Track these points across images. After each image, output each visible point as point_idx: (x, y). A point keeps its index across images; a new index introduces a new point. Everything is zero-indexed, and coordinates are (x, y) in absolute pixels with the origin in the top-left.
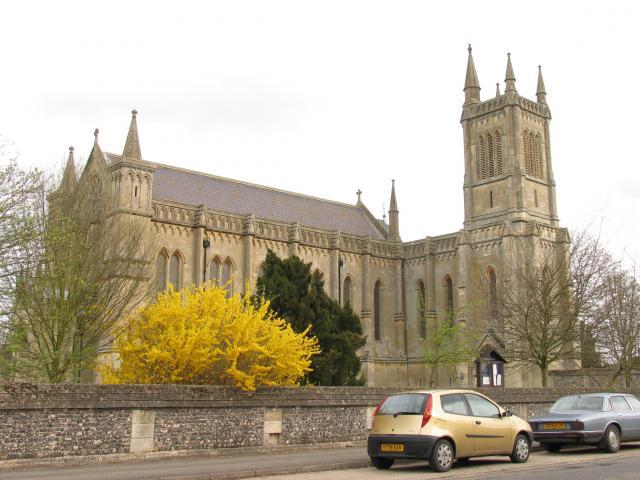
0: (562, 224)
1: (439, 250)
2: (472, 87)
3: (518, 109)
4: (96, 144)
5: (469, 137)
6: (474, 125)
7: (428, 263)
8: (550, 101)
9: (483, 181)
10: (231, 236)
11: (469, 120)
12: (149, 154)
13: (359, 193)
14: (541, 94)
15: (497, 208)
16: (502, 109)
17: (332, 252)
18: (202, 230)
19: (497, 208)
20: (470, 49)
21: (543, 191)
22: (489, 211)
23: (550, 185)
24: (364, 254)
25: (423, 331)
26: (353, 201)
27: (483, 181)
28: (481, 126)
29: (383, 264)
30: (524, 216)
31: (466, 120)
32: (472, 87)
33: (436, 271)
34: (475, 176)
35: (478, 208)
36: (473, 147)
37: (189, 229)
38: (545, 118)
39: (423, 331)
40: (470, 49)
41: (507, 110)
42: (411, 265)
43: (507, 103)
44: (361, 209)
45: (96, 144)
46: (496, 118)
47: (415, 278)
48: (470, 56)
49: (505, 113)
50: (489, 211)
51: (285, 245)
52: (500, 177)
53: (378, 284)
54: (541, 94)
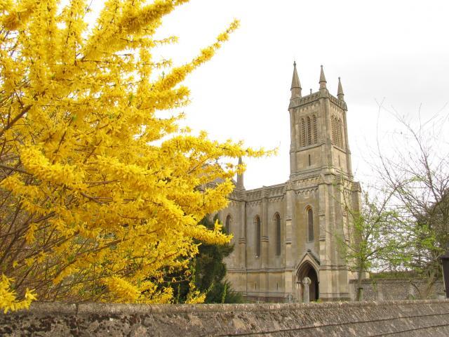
0: (355, 180)
2: (296, 87)
6: (298, 112)
8: (346, 98)
15: (314, 166)
19: (314, 166)
20: (295, 65)
21: (343, 156)
22: (308, 168)
23: (348, 153)
28: (303, 112)
31: (293, 109)
40: (295, 65)
43: (320, 97)
46: (313, 107)
54: (340, 94)
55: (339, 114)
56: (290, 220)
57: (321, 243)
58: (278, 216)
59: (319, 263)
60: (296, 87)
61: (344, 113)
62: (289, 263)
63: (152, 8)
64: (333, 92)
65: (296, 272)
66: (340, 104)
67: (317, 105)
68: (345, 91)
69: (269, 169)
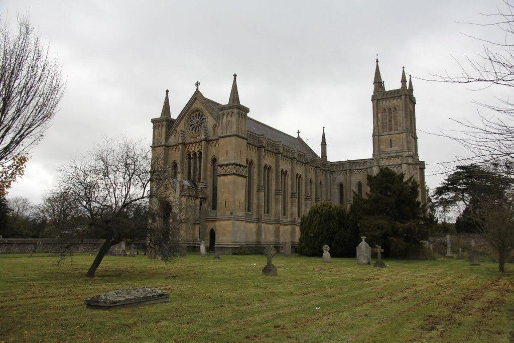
1: (354, 168)
2: (378, 82)
5: (377, 109)
6: (381, 103)
9: (386, 133)
11: (378, 100)
15: (395, 149)
16: (401, 96)
17: (306, 165)
18: (263, 149)
19: (395, 149)
20: (377, 62)
22: (389, 149)
24: (185, 145)
25: (93, 304)
27: (386, 133)
28: (384, 104)
32: (378, 82)
33: (352, 179)
34: (381, 130)
35: (382, 147)
36: (380, 115)
37: (256, 148)
39: (93, 304)
40: (377, 62)
41: (403, 97)
42: (334, 175)
46: (395, 101)
47: (337, 181)
48: (377, 66)
49: (401, 98)
50: (389, 149)
51: (274, 154)
53: (310, 181)
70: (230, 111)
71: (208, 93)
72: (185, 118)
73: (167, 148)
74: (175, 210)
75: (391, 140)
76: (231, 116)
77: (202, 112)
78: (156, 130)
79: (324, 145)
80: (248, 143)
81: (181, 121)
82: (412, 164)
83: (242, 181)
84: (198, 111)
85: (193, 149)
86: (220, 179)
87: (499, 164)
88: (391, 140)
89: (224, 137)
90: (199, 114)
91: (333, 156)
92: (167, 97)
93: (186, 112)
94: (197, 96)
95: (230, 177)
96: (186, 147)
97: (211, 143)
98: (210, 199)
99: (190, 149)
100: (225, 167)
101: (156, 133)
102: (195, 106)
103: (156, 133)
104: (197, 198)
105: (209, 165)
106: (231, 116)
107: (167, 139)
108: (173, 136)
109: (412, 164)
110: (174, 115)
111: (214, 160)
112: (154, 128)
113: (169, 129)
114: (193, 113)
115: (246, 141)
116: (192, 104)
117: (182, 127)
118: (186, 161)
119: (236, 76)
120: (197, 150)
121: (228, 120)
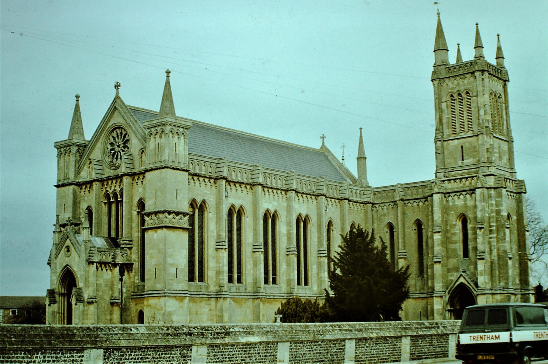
0: (519, 177)
2: (441, 46)
3: (486, 73)
4: (117, 97)
7: (72, 159)
8: (507, 64)
10: (243, 186)
12: (184, 110)
13: (117, 86)
14: (499, 56)
15: (468, 161)
19: (468, 161)
21: (505, 146)
23: (510, 141)
26: (317, 145)
28: (451, 85)
29: (356, 209)
30: (493, 170)
31: (436, 78)
38: (505, 81)
40: (439, 14)
43: (475, 68)
44: (323, 154)
45: (117, 97)
46: (466, 81)
52: (470, 134)
53: (330, 224)
54: (499, 56)
55: (498, 87)
56: (439, 262)
57: (479, 262)
58: (419, 224)
59: (477, 286)
60: (441, 46)
61: (505, 84)
62: (438, 286)
63: (30, 305)
64: (490, 58)
65: (448, 297)
66: (499, 73)
67: (472, 79)
68: (505, 53)
69: (403, 156)
70: (159, 129)
71: (130, 99)
72: (100, 140)
73: (500, 56)
74: (81, 284)
75: (462, 147)
76: (161, 137)
77: (125, 130)
78: (62, 160)
79: (361, 158)
80: (189, 174)
81: (96, 142)
82: (495, 188)
83: (185, 236)
84: (119, 128)
85: (113, 188)
86: (148, 235)
87: (193, 333)
88: (462, 147)
89: (151, 170)
90: (121, 133)
91: (378, 178)
92: (168, 83)
93: (103, 130)
94: (116, 106)
95: (159, 231)
96: (103, 185)
97: (136, 178)
98: (136, 265)
99: (108, 189)
100: (153, 216)
101: (62, 164)
102: (117, 119)
103: (62, 164)
104: (115, 265)
105: (135, 213)
106: (161, 137)
107: (78, 171)
108: (86, 168)
109: (495, 188)
110: (88, 136)
111: (141, 204)
112: (59, 155)
113: (81, 157)
114: (112, 131)
115: (187, 173)
116: (111, 117)
117: (97, 154)
118: (105, 208)
119: (119, 86)
120: (118, 189)
121: (157, 143)
